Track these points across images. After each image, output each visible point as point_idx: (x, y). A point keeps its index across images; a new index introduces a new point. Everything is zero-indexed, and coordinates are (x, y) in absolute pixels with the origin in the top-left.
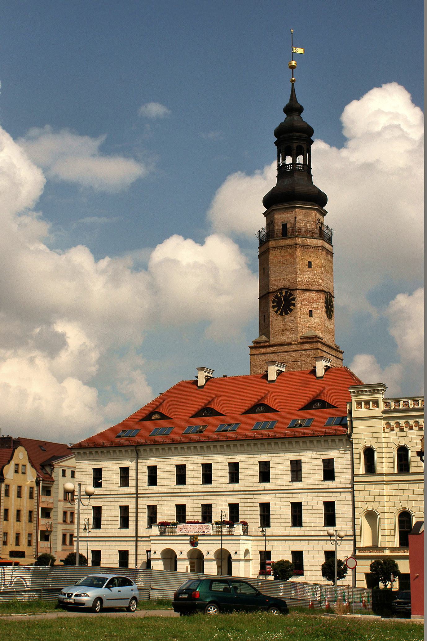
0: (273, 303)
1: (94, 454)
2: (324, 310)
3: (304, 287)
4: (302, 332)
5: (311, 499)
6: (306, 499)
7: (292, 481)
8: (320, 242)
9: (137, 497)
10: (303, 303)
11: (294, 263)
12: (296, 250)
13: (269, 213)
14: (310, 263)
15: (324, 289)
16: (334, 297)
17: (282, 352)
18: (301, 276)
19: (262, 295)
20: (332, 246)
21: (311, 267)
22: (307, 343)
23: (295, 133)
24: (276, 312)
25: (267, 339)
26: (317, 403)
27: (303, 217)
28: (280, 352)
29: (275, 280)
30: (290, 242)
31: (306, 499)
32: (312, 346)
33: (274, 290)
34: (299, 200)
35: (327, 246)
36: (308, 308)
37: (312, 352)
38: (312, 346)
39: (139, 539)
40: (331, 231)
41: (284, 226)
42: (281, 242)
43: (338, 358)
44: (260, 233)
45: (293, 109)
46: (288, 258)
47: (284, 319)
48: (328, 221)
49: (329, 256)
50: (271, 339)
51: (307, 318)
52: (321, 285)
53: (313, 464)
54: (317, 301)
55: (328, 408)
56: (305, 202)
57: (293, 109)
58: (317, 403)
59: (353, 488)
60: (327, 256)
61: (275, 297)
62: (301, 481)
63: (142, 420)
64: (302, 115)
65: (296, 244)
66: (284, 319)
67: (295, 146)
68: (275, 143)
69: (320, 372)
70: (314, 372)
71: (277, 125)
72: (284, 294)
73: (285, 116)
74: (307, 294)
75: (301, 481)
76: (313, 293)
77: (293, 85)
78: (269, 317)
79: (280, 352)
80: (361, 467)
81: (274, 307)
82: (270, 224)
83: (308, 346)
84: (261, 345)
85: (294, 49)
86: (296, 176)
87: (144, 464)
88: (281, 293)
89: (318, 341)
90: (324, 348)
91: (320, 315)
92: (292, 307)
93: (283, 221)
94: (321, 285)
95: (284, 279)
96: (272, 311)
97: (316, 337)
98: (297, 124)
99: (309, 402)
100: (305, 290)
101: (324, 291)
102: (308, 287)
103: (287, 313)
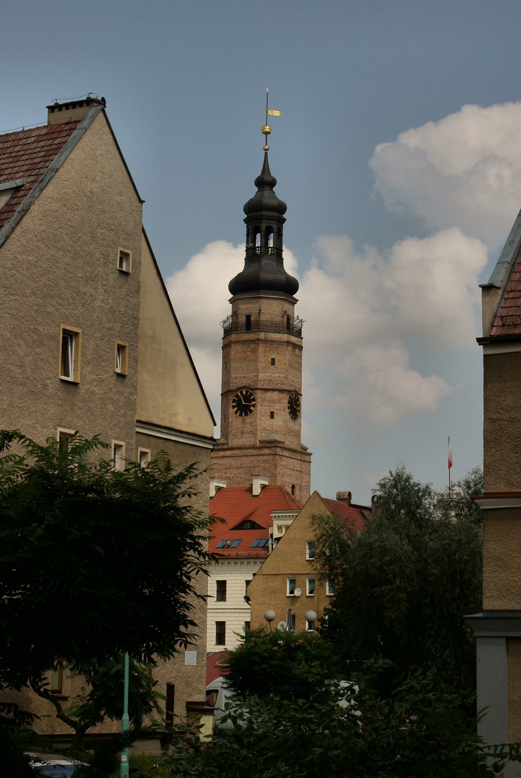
0: (233, 402)
2: (288, 411)
3: (266, 387)
4: (262, 436)
5: (234, 619)
6: (229, 619)
7: (218, 600)
8: (285, 337)
10: (264, 404)
11: (256, 360)
12: (258, 346)
13: (234, 301)
14: (273, 360)
15: (288, 388)
16: (301, 395)
17: (241, 456)
18: (263, 374)
19: (225, 391)
21: (274, 365)
22: (266, 447)
23: (264, 213)
24: (236, 412)
25: (225, 441)
26: (247, 524)
27: (270, 308)
28: (238, 456)
29: (236, 378)
30: (252, 336)
31: (229, 619)
32: (271, 452)
33: (234, 389)
34: (264, 289)
35: (294, 339)
36: (269, 410)
37: (270, 458)
38: (271, 452)
41: (248, 317)
42: (244, 337)
43: (304, 461)
44: (225, 322)
45: (265, 182)
46: (249, 354)
48: (298, 311)
49: (297, 350)
50: (230, 441)
51: (268, 420)
52: (284, 384)
53: (237, 585)
54: (279, 401)
55: (257, 529)
56: (271, 292)
57: (265, 182)
58: (247, 524)
60: (294, 351)
61: (235, 397)
62: (225, 601)
64: (275, 189)
65: (258, 340)
67: (264, 226)
68: (244, 220)
69: (257, 490)
70: (250, 490)
71: (247, 201)
72: (244, 393)
73: (256, 189)
74: (269, 395)
75: (225, 601)
76: (276, 393)
77: (266, 154)
78: (228, 418)
79: (238, 456)
81: (234, 407)
82: (235, 314)
83: (267, 451)
84: (220, 447)
85: (269, 111)
86: (264, 261)
88: (241, 393)
89: (276, 447)
90: (286, 453)
91: (283, 416)
92: (252, 408)
93: (247, 312)
94: (284, 384)
95: (245, 377)
96: (232, 411)
97: (276, 441)
98: (267, 201)
99: (240, 521)
100: (266, 390)
101: (288, 391)
102: (271, 387)
103: (246, 415)
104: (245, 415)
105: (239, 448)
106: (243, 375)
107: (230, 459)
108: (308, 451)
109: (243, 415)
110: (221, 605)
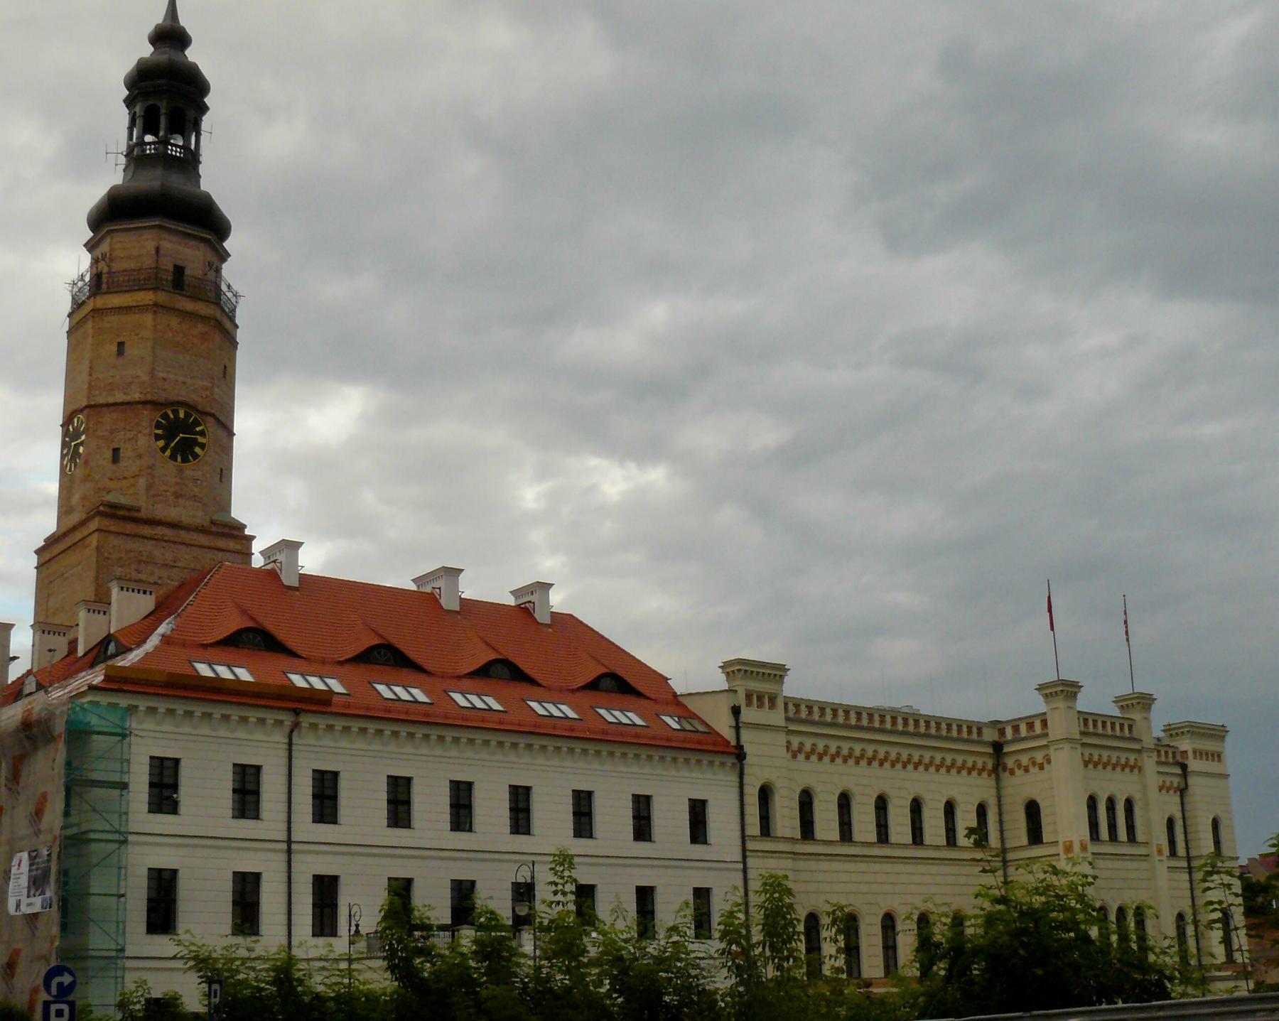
1: (321, 732)
9: (289, 851)
20: (237, 327)
29: (164, 379)
39: (1010, 856)
40: (235, 295)
45: (170, 36)
47: (181, 471)
57: (170, 36)
59: (744, 863)
61: (162, 417)
63: (638, 694)
66: (181, 471)
73: (152, 49)
80: (754, 827)
87: (321, 749)
92: (197, 450)
103: (185, 460)
104: (183, 461)
105: (174, 525)
106: (181, 379)
107: (151, 542)
108: (247, 532)
109: (179, 459)
110: (164, 822)
